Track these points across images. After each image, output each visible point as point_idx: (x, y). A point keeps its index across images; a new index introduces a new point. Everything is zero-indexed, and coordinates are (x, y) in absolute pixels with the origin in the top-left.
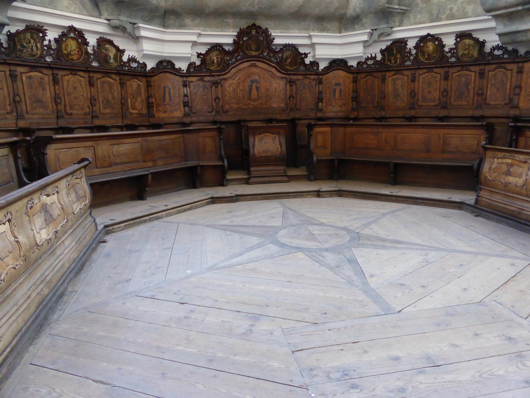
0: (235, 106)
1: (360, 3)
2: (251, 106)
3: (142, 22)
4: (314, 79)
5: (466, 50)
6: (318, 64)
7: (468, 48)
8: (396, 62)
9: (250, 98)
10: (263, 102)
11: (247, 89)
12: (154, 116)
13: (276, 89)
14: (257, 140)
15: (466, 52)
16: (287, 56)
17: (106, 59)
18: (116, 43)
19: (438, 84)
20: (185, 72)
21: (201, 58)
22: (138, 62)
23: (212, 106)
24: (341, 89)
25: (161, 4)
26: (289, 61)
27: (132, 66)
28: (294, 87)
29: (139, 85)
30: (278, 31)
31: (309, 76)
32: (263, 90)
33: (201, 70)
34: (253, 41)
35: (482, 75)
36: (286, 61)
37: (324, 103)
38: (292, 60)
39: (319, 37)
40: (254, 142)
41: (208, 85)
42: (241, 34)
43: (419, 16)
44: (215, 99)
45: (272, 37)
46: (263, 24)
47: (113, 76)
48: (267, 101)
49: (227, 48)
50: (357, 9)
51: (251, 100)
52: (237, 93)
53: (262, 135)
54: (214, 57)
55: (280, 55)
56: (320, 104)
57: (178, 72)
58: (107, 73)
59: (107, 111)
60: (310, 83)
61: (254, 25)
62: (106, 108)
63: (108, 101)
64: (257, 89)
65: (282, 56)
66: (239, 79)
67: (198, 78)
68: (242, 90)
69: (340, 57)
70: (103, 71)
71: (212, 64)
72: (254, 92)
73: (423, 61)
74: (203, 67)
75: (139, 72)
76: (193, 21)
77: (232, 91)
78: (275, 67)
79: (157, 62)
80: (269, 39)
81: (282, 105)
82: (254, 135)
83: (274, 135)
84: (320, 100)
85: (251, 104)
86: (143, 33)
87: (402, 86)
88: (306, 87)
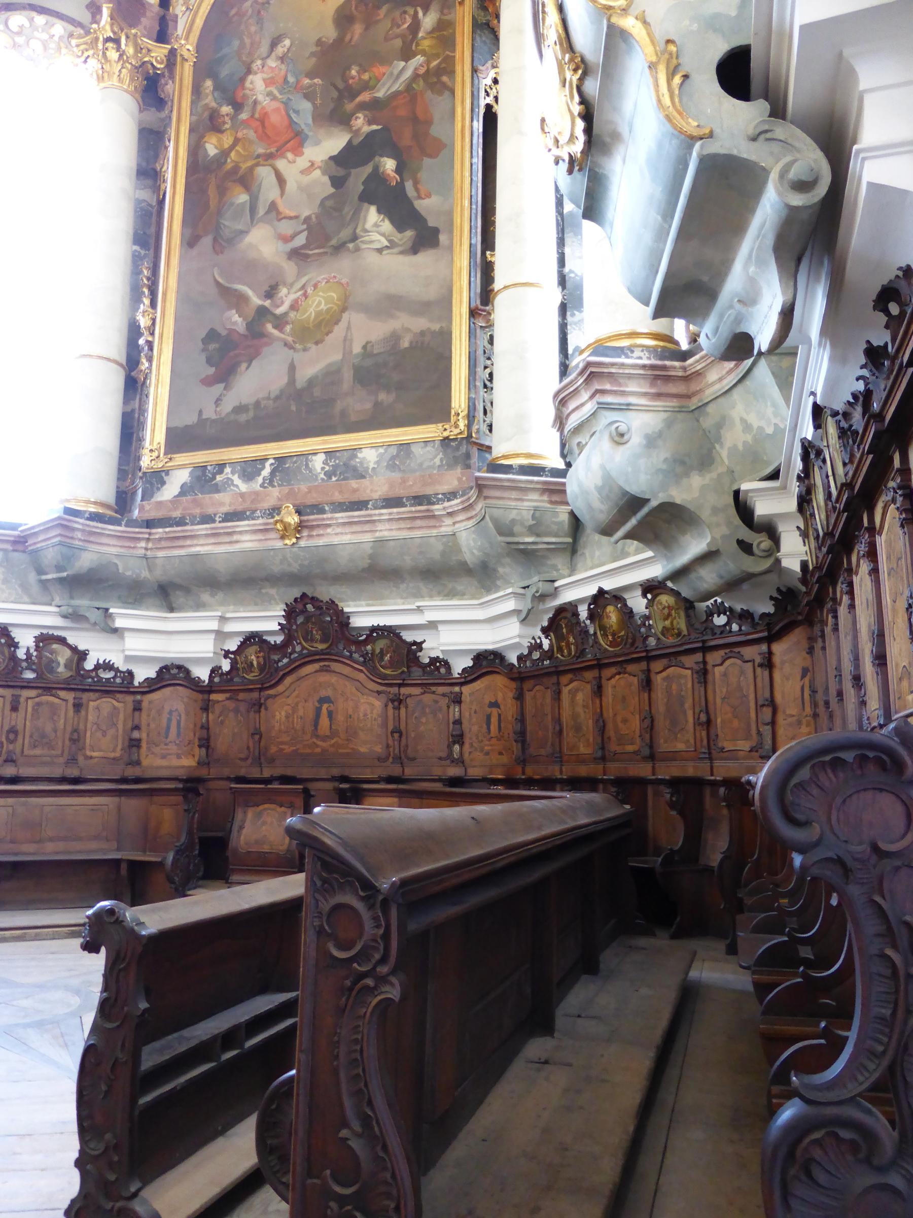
0: (288, 749)
1: (474, 540)
2: (318, 750)
3: (120, 604)
4: (444, 695)
5: (666, 619)
6: (447, 664)
7: (669, 615)
8: (570, 653)
9: (315, 734)
10: (340, 742)
11: (311, 716)
12: (138, 763)
13: (365, 715)
14: (250, 815)
15: (667, 623)
16: (382, 650)
17: (51, 665)
18: (71, 641)
19: (637, 699)
20: (207, 681)
21: (230, 658)
22: (117, 670)
23: (248, 748)
24: (499, 715)
25: (143, 576)
26: (387, 658)
27: (102, 676)
28: (403, 711)
29: (115, 708)
30: (363, 603)
31: (433, 689)
32: (340, 718)
33: (232, 679)
34: (316, 626)
35: (703, 674)
36: (382, 659)
37: (467, 747)
38: (398, 659)
39: (435, 608)
40: (244, 821)
41: (243, 707)
42: (290, 613)
43: (597, 553)
44: (392, 733)
45: (346, 615)
46: (325, 592)
47: (62, 694)
48: (348, 740)
49: (271, 639)
50: (475, 551)
51: (317, 737)
52: (293, 721)
53: (261, 807)
54: (253, 656)
55: (369, 647)
56: (457, 747)
57: (193, 684)
58: (48, 690)
59: (37, 752)
60: (436, 702)
61: (304, 595)
62: (35, 747)
63: (43, 736)
64: (330, 714)
65: (373, 650)
66: (297, 697)
67: (228, 695)
68: (301, 718)
69: (490, 647)
70: (419, 682)
71: (255, 670)
72: (324, 721)
73: (606, 649)
74: (234, 673)
75: (120, 685)
76: (213, 595)
77: (283, 719)
78: (361, 671)
79: (157, 669)
80: (342, 620)
81: (273, 749)
82: (247, 805)
83: (283, 809)
84: (459, 738)
85: (317, 746)
86: (119, 623)
87: (584, 706)
88: (427, 710)
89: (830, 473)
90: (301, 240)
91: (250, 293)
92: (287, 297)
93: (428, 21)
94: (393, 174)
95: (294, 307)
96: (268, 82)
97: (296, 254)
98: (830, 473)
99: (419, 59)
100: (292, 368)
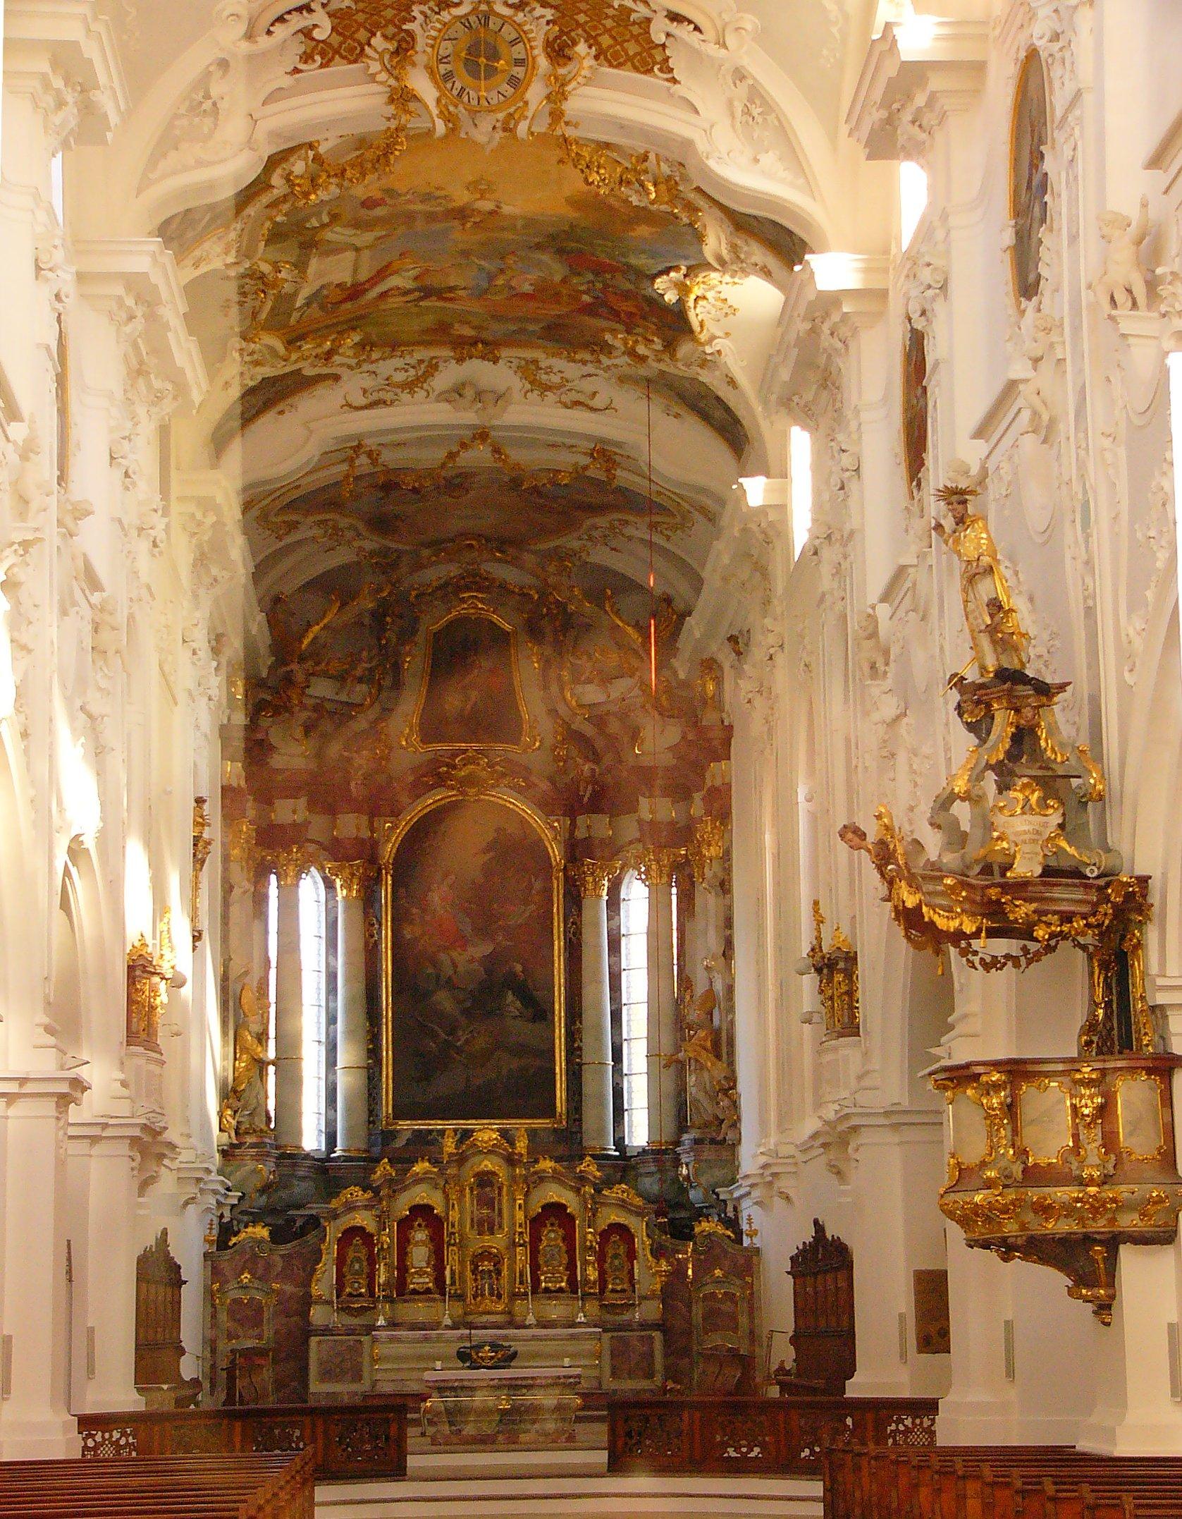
89: (270, 499)
90: (468, 1004)
91: (440, 1031)
92: (463, 1036)
93: (538, 885)
94: (577, 215)
95: (467, 1041)
96: (443, 899)
97: (466, 1012)
98: (270, 499)
99: (533, 907)
100: (468, 1080)
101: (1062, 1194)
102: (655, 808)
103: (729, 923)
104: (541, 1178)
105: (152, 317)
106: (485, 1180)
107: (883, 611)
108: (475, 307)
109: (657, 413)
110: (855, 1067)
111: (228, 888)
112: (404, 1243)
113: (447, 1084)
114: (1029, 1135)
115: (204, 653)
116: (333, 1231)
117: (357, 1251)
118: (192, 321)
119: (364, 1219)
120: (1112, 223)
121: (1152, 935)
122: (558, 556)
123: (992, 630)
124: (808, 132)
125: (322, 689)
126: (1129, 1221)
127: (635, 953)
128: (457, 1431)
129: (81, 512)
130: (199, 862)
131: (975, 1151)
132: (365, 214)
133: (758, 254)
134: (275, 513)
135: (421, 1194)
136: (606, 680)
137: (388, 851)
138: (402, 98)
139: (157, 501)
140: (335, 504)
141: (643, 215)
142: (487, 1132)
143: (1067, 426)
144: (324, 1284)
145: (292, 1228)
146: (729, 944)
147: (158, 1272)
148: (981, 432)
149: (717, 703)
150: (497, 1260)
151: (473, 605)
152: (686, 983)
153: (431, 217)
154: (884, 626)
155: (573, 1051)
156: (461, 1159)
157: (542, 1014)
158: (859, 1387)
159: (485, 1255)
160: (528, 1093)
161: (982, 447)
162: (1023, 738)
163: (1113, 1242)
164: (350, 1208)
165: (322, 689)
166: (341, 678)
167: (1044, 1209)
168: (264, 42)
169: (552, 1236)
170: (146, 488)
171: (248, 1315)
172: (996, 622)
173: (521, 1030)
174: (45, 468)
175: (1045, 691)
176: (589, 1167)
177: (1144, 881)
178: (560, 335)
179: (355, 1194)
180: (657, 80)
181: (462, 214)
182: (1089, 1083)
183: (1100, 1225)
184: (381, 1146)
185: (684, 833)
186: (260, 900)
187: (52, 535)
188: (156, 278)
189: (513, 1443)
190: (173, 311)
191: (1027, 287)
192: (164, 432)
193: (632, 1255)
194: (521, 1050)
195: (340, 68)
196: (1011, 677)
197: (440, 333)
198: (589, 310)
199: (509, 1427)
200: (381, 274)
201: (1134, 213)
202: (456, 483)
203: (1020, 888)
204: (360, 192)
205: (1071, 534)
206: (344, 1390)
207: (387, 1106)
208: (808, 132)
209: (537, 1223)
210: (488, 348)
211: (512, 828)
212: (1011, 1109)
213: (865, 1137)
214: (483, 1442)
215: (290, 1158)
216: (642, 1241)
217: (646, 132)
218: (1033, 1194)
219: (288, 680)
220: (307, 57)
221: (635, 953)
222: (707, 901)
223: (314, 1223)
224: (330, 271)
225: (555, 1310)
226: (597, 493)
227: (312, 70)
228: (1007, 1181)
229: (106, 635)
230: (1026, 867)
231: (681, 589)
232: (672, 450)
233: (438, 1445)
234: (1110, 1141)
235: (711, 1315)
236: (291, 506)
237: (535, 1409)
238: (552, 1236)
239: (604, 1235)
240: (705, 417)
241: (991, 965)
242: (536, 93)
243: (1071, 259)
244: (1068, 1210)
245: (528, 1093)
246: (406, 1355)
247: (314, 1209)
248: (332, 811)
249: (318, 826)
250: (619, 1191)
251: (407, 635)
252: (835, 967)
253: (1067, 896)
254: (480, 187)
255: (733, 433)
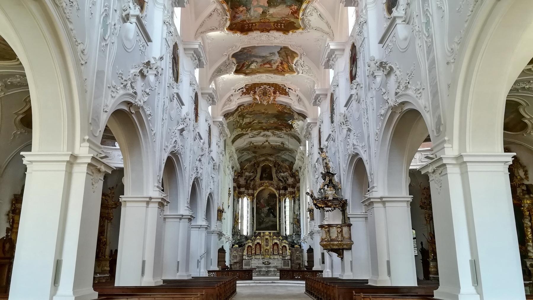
101: (335, 243)
102: (290, 189)
103: (300, 205)
104: (274, 239)
105: (222, 126)
106: (267, 239)
107: (316, 164)
108: (265, 125)
109: (289, 138)
110: (314, 225)
111: (234, 200)
112: (256, 247)
113: (263, 226)
114: (331, 235)
115: (231, 169)
116: (247, 246)
117: (250, 249)
118: (228, 127)
119: (250, 244)
120: (341, 114)
121: (348, 208)
122: (278, 156)
123: (326, 166)
124: (306, 102)
125: (247, 174)
126: (345, 247)
127: (288, 209)
128: (260, 273)
129: (211, 151)
130: (229, 196)
131: (324, 236)
132: (250, 113)
133: (302, 118)
134: (241, 151)
135: (258, 241)
136: (284, 172)
137: (255, 195)
138: (255, 99)
139: (223, 149)
140: (249, 150)
141: (286, 113)
142: (267, 232)
143: (336, 140)
144: (245, 253)
145: (241, 245)
146: (300, 208)
147: (222, 251)
148: (327, 141)
149: (298, 175)
150: (268, 250)
151: (267, 163)
152: (294, 213)
153: (259, 114)
154: (317, 166)
155: (279, 222)
156: (263, 236)
157: (275, 217)
158: (314, 269)
159: (267, 249)
160: (273, 227)
161: (327, 142)
162: (330, 181)
163: (343, 249)
164: (249, 243)
165: (247, 174)
166: (249, 172)
167: (333, 245)
168: (237, 92)
169: (275, 247)
170: (222, 148)
171: (235, 257)
172: (326, 166)
173: (273, 219)
174: (207, 145)
175: (333, 175)
176: (281, 238)
177: (346, 200)
178: (277, 128)
179: (250, 241)
180: (287, 96)
181: (263, 113)
182: (339, 228)
183: (341, 247)
184: (255, 235)
185: (294, 193)
186: (238, 201)
187: (207, 154)
188: (223, 122)
189: (268, 275)
190: (225, 126)
191: (332, 122)
192: (225, 141)
193: (286, 250)
194: (273, 221)
195: (247, 95)
196: (328, 173)
197: (261, 128)
198: (280, 125)
199: (267, 273)
200: (253, 121)
201: (343, 112)
202: (264, 147)
203: (330, 201)
204: (250, 110)
205: (337, 154)
206: (248, 267)
207: (255, 229)
208: (306, 102)
209: (273, 245)
210: (267, 130)
211: (272, 192)
212: (329, 231)
213: (315, 234)
214: (264, 275)
215: (242, 236)
216: (288, 248)
217: (286, 103)
218: (332, 243)
219: (242, 172)
220: (243, 94)
221: (288, 209)
222: (297, 202)
223: (244, 244)
224: (247, 120)
225: (276, 257)
226: (281, 149)
227: (243, 96)
228: (328, 241)
229: (215, 167)
230: (330, 198)
231: (293, 161)
232: (290, 143)
233: (258, 275)
234: (342, 236)
235: (297, 258)
236: (243, 150)
237: (271, 271)
238: (275, 247)
239: (283, 247)
240: (296, 139)
241: (327, 211)
242: (272, 98)
243: (337, 118)
244: (337, 245)
245: (273, 227)
246: (256, 262)
247: (245, 243)
248: (279, 190)
249: (246, 191)
250: (284, 241)
251: (258, 167)
252: (311, 211)
253: (336, 202)
254: (265, 110)
255: (299, 140)
